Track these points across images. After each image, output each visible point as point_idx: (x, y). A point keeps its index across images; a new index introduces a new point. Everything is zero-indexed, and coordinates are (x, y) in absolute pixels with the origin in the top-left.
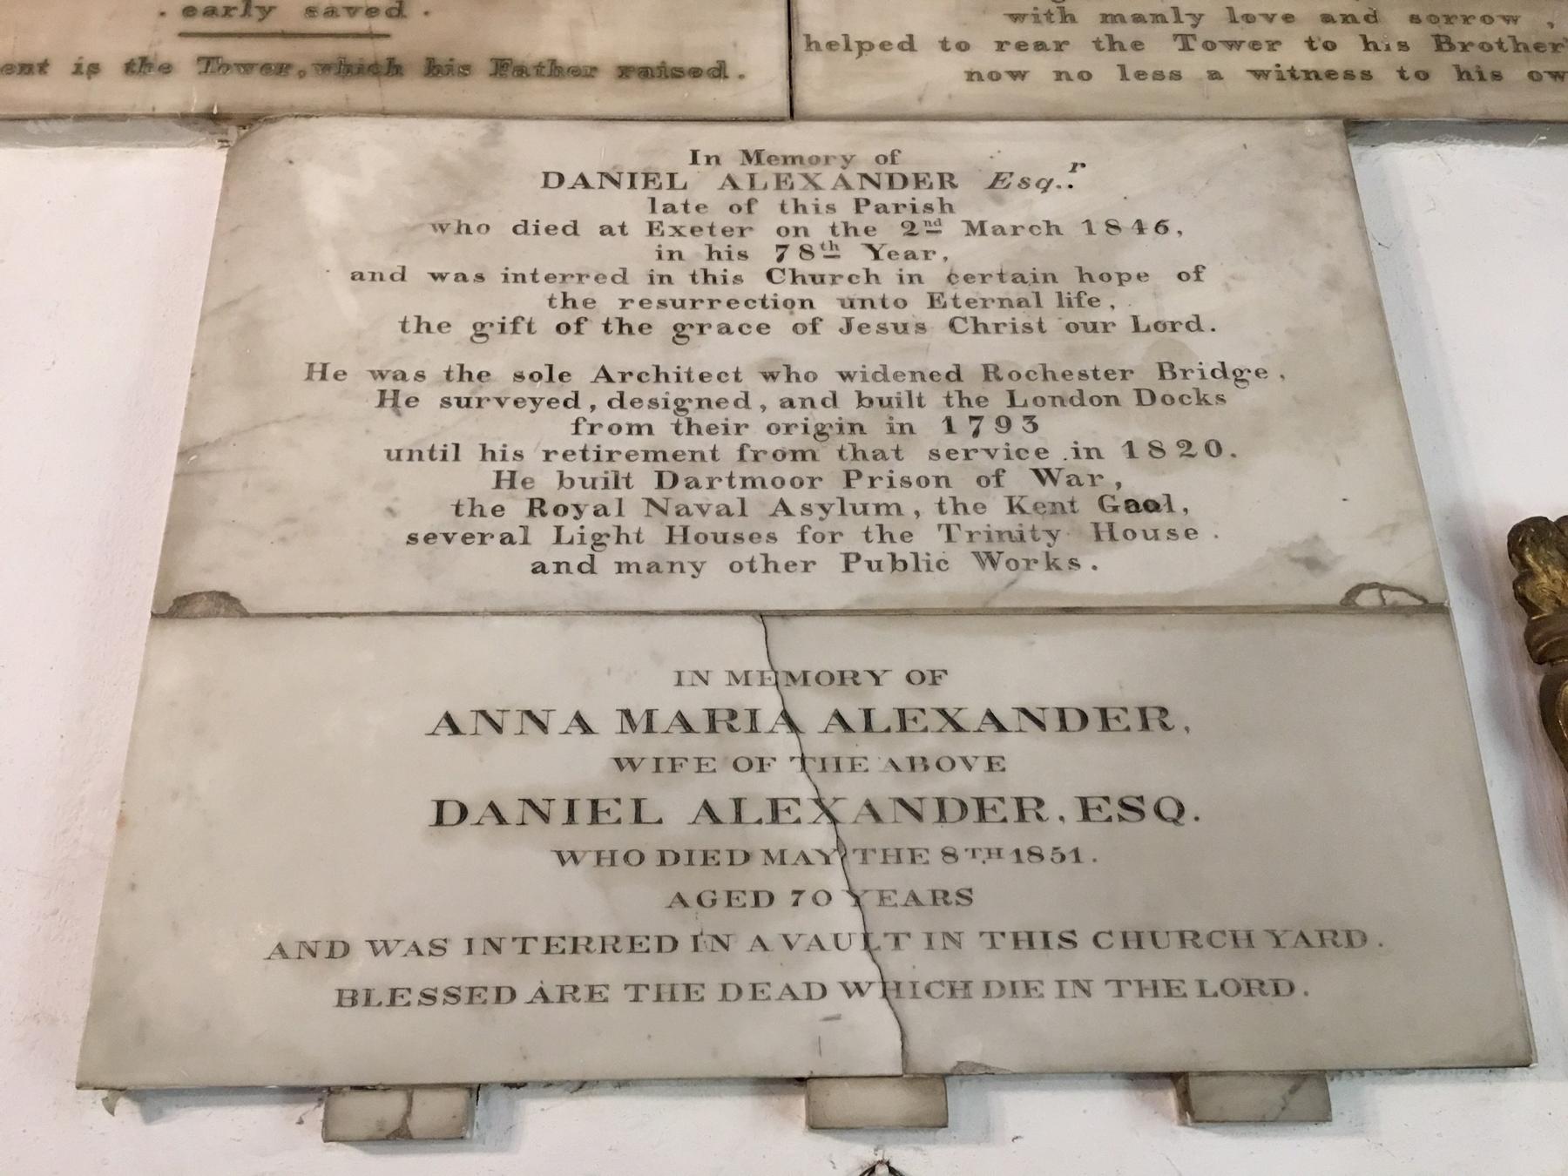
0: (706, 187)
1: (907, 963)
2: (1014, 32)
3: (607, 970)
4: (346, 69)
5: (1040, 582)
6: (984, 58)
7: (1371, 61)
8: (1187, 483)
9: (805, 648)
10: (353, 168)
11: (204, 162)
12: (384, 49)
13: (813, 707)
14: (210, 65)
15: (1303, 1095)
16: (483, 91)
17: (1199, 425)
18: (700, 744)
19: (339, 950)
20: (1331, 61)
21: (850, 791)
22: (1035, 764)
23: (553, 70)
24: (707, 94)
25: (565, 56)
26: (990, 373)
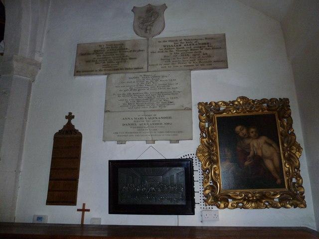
0: (141, 78)
1: (153, 134)
2: (165, 63)
3: (134, 134)
4: (115, 70)
5: (163, 108)
6: (162, 66)
7: (194, 64)
8: (175, 101)
9: (147, 113)
10: (116, 77)
11: (105, 77)
12: (117, 68)
13: (147, 117)
14: (105, 70)
15: (177, 141)
16: (125, 71)
17: (176, 96)
18: (140, 120)
19: (117, 133)
20: (190, 64)
21: (149, 123)
22: (162, 121)
23: (130, 69)
24: (142, 70)
25: (131, 67)
26: (161, 92)
